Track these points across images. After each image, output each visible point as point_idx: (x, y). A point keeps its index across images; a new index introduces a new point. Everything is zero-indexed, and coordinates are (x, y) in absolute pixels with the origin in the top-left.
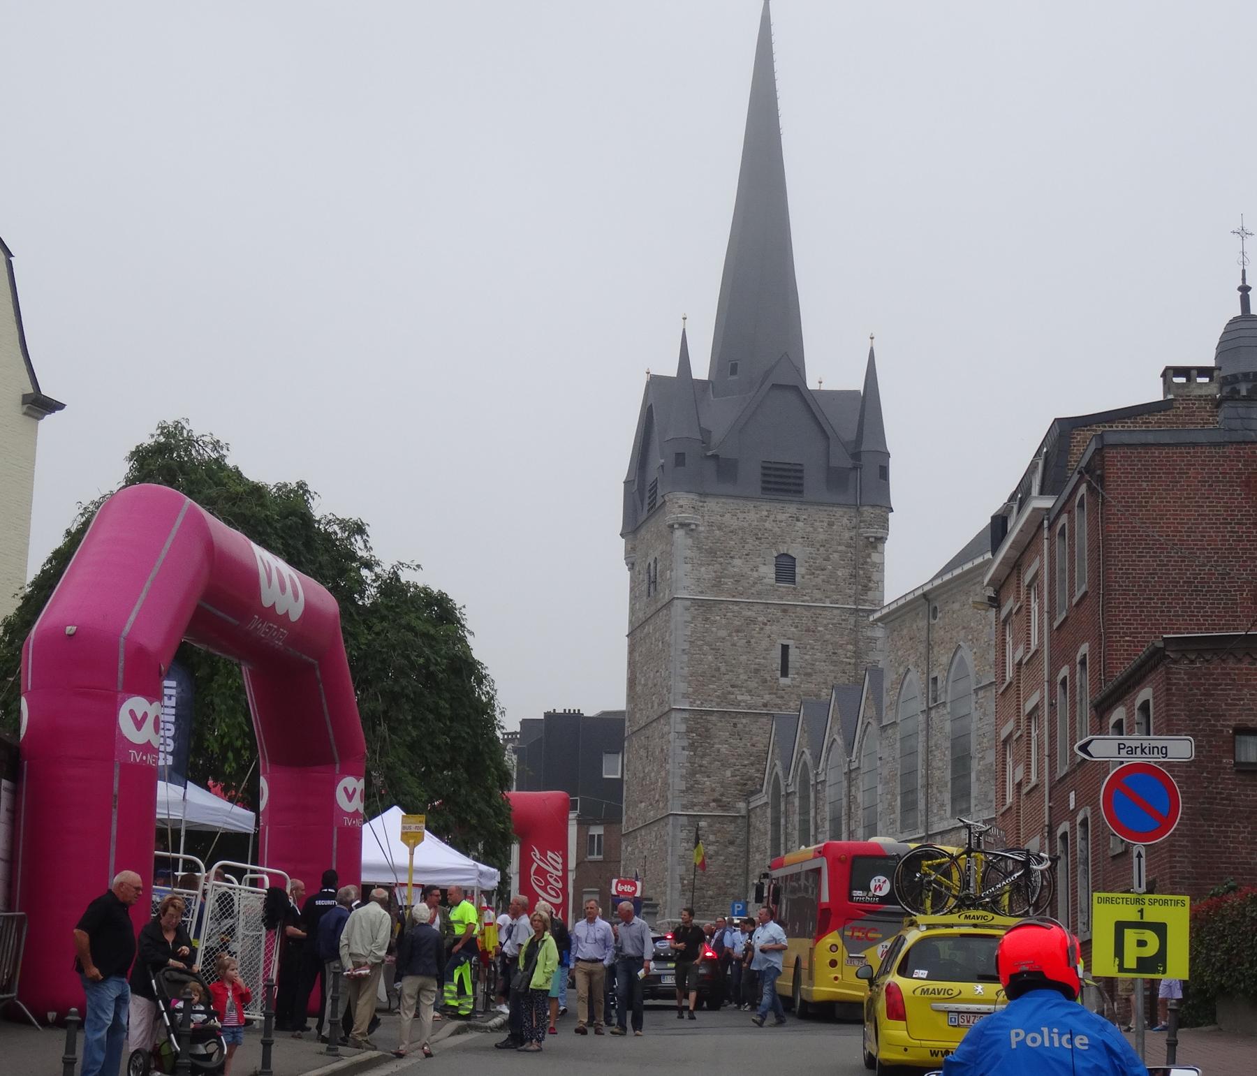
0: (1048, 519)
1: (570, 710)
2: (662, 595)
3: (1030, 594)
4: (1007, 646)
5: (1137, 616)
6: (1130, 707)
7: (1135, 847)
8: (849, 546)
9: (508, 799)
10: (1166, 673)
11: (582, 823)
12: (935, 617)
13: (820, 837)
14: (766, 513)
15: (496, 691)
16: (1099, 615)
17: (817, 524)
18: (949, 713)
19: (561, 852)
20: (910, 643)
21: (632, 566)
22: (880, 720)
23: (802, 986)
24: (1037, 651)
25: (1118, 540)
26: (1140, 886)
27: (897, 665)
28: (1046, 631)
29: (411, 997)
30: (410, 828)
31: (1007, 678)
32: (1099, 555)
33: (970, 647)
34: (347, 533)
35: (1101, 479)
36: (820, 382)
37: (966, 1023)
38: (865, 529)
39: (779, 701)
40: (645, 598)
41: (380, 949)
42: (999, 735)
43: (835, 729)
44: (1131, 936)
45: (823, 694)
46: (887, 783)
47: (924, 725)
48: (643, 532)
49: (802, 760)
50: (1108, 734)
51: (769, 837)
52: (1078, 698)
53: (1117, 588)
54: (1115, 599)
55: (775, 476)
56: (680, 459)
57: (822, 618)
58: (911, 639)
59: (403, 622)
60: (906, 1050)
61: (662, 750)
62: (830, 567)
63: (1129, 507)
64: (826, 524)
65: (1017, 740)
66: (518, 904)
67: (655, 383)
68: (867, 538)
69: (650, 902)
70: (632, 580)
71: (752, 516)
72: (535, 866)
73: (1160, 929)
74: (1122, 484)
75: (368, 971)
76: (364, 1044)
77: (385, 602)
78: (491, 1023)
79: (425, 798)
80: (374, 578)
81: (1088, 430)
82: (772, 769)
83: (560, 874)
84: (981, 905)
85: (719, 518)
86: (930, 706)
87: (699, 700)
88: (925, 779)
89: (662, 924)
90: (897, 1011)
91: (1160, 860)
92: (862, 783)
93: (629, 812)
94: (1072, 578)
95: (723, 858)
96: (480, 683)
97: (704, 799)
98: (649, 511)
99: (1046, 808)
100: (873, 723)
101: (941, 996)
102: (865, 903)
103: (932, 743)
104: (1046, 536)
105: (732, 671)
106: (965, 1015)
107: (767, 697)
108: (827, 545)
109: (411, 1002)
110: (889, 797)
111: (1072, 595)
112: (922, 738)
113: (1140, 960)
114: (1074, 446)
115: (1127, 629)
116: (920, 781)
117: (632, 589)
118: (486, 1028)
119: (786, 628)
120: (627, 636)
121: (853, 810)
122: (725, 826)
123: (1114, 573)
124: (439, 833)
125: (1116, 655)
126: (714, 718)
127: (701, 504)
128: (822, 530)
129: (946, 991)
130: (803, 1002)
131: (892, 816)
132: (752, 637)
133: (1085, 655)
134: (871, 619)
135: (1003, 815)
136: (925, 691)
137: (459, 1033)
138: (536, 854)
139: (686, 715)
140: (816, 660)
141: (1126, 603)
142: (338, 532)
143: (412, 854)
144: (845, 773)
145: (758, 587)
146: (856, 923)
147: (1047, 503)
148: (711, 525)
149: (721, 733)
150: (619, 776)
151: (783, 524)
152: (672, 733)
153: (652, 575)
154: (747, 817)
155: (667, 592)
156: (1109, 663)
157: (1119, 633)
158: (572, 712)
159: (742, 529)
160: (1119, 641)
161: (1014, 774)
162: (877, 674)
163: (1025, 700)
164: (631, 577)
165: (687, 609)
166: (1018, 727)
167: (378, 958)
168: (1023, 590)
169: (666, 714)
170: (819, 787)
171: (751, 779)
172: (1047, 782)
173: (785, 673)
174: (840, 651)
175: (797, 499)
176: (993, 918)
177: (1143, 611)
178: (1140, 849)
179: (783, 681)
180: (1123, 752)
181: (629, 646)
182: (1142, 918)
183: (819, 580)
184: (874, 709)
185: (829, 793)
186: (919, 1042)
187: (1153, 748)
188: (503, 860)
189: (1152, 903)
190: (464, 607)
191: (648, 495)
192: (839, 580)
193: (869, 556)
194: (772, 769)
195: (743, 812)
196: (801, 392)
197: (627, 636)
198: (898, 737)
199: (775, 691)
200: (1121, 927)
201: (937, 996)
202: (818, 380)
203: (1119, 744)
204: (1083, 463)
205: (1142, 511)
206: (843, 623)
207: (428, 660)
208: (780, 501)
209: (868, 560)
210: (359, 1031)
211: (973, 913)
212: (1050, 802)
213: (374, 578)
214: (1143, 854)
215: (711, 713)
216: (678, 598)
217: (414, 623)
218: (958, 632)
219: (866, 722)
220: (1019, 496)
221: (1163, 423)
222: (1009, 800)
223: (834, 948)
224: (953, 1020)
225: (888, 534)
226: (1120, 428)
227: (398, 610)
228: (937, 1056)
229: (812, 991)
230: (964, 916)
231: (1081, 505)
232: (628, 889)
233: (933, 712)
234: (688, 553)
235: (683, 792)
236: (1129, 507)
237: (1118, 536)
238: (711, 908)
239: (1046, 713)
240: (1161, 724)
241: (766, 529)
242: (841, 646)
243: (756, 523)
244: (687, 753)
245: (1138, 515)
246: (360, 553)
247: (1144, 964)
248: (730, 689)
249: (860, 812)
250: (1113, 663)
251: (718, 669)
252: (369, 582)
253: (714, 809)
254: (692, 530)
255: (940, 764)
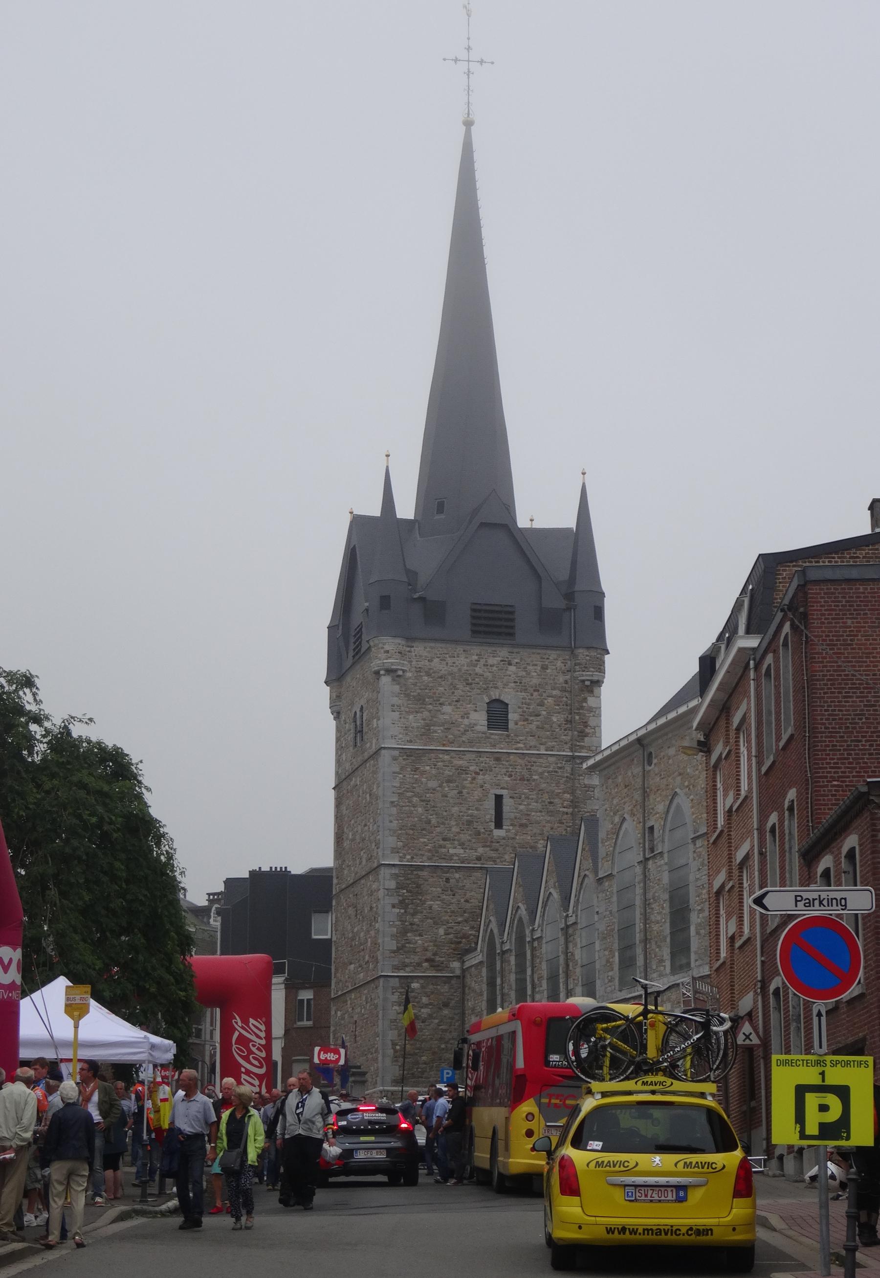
0: (754, 659)
1: (276, 868)
2: (368, 745)
3: (739, 737)
4: (718, 792)
5: (845, 759)
6: (837, 855)
7: (814, 1006)
8: (563, 690)
9: (190, 965)
10: (872, 819)
11: (291, 988)
12: (650, 764)
13: (537, 997)
14: (476, 658)
15: (175, 850)
16: (805, 759)
17: (530, 668)
18: (666, 864)
19: (264, 1019)
20: (626, 790)
21: (337, 715)
22: (596, 872)
23: (499, 1159)
24: (746, 797)
25: (823, 680)
26: (821, 1047)
27: (612, 814)
28: (754, 777)
29: (60, 1183)
30: (74, 999)
31: (719, 826)
32: (804, 696)
33: (686, 794)
34: (14, 686)
35: (805, 617)
36: (532, 520)
37: (643, 1198)
38: (581, 673)
39: (493, 854)
40: (351, 748)
41: (26, 1131)
42: (712, 886)
43: (551, 883)
44: (812, 1101)
45: (540, 846)
46: (605, 938)
47: (642, 877)
48: (348, 679)
49: (517, 916)
50: (840, 885)
51: (485, 998)
52: (787, 846)
53: (823, 730)
54: (821, 742)
55: (485, 618)
56: (385, 602)
57: (537, 766)
58: (626, 786)
59: (75, 779)
60: (580, 1227)
61: (371, 908)
62: (544, 713)
63: (834, 645)
64: (539, 668)
65: (729, 891)
66: (190, 1080)
67: (359, 523)
68: (583, 681)
69: (359, 1070)
70: (338, 730)
71: (462, 660)
72: (236, 1034)
73: (843, 1092)
74: (826, 621)
75: (13, 1155)
76: (10, 1235)
77: (56, 759)
78: (164, 1207)
79: (99, 965)
80: (44, 733)
81: (794, 566)
82: (487, 925)
83: (263, 1042)
84: (660, 1070)
85: (427, 663)
86: (647, 856)
87: (409, 854)
88: (642, 935)
89: (374, 1092)
90: (571, 1187)
91: (870, 1017)
92: (580, 939)
93: (338, 975)
94: (778, 720)
95: (437, 1021)
96: (158, 844)
97: (416, 959)
98: (354, 657)
99: (759, 963)
100: (590, 876)
101: (617, 1168)
102: (562, 1068)
103: (650, 895)
104: (752, 677)
105: (443, 824)
106: (643, 1189)
107: (481, 850)
108: (541, 690)
109: (60, 1188)
110: (607, 953)
111: (778, 739)
112: (639, 890)
113: (822, 1126)
114: (780, 583)
115: (835, 773)
116: (638, 937)
117: (338, 740)
118: (156, 1213)
119: (499, 777)
120: (334, 788)
121: (571, 968)
122: (439, 987)
123: (819, 715)
124: (114, 1005)
125: (824, 800)
126: (424, 873)
127: (408, 649)
128: (536, 674)
129: (622, 1163)
130: (500, 1174)
131: (610, 974)
132: (464, 787)
133: (793, 801)
134: (585, 766)
135: (717, 970)
136: (641, 841)
137: (122, 1220)
138: (237, 1022)
139: (395, 871)
140: (532, 810)
141: (833, 746)
142: (5, 684)
143: (76, 1027)
144: (562, 929)
145: (470, 735)
146: (553, 1090)
147: (753, 642)
148: (419, 670)
149: (434, 889)
150: (329, 937)
151: (495, 668)
152: (382, 890)
153: (358, 723)
154: (462, 978)
155: (374, 741)
156: (817, 809)
157: (826, 777)
158: (273, 870)
159: (451, 674)
160: (827, 786)
161: (727, 928)
162: (593, 822)
163: (737, 849)
164: (337, 727)
165: (395, 759)
166: (730, 877)
167: (23, 1140)
168: (732, 734)
169: (375, 870)
170: (536, 944)
171: (465, 936)
172: (758, 935)
173: (499, 824)
174: (556, 801)
175: (509, 642)
176: (672, 1084)
177: (850, 754)
178: (819, 1007)
179: (498, 833)
180: (801, 905)
181: (336, 799)
182: (823, 1081)
183: (533, 727)
184: (591, 861)
185: (546, 950)
186: (593, 1218)
187: (832, 899)
188: (184, 1031)
189: (834, 1064)
190: (141, 762)
191: (352, 640)
192: (554, 725)
193: (585, 700)
194: (487, 925)
195: (458, 972)
196: (510, 530)
197: (334, 788)
198: (615, 891)
199: (488, 844)
200: (801, 1091)
201: (612, 1169)
202: (530, 517)
203: (796, 896)
204: (786, 601)
205: (847, 649)
206: (559, 770)
207: (101, 819)
208: (490, 644)
209: (584, 704)
210: (4, 1222)
211: (650, 1078)
212: (762, 955)
213: (44, 733)
214: (824, 1013)
215: (421, 868)
216: (385, 748)
217: (87, 780)
218: (674, 779)
219: (582, 874)
220: (727, 635)
221: (872, 558)
222: (723, 954)
223: (530, 1117)
224: (630, 1194)
225: (604, 677)
226: (827, 564)
227: (69, 767)
228: (613, 1233)
229: (507, 1163)
230: (641, 1082)
231: (785, 644)
232: (331, 1056)
233: (650, 862)
234: (396, 700)
235: (394, 952)
236: (834, 645)
237: (824, 675)
238: (426, 1075)
239: (756, 862)
240: (868, 872)
241: (476, 674)
242: (558, 794)
243: (465, 668)
244: (397, 910)
245: (844, 654)
246: (28, 707)
247: (827, 1131)
248: (442, 842)
249: (578, 970)
250: (820, 809)
251: (429, 822)
252: (38, 737)
253: (427, 969)
254: (399, 676)
255: (659, 918)
